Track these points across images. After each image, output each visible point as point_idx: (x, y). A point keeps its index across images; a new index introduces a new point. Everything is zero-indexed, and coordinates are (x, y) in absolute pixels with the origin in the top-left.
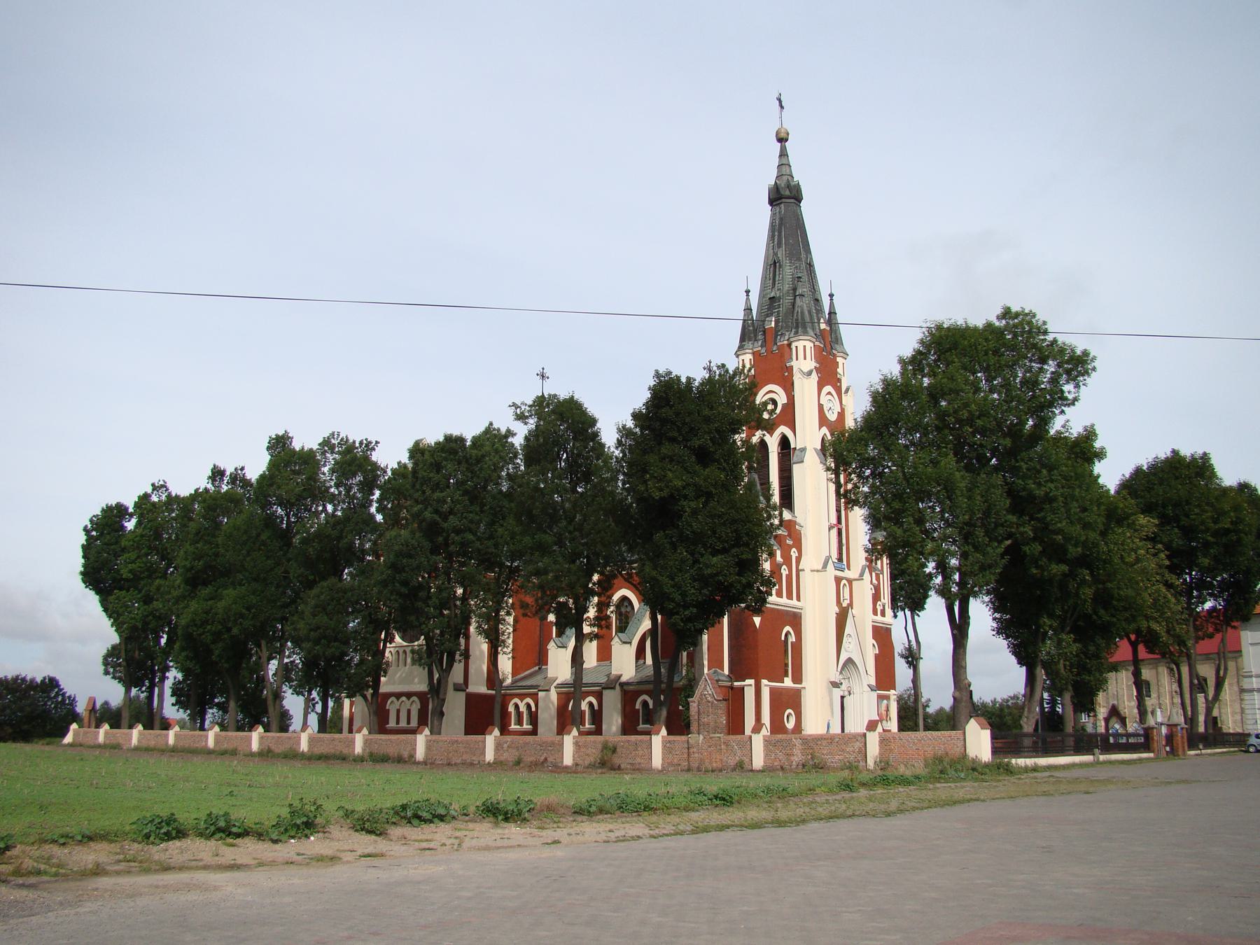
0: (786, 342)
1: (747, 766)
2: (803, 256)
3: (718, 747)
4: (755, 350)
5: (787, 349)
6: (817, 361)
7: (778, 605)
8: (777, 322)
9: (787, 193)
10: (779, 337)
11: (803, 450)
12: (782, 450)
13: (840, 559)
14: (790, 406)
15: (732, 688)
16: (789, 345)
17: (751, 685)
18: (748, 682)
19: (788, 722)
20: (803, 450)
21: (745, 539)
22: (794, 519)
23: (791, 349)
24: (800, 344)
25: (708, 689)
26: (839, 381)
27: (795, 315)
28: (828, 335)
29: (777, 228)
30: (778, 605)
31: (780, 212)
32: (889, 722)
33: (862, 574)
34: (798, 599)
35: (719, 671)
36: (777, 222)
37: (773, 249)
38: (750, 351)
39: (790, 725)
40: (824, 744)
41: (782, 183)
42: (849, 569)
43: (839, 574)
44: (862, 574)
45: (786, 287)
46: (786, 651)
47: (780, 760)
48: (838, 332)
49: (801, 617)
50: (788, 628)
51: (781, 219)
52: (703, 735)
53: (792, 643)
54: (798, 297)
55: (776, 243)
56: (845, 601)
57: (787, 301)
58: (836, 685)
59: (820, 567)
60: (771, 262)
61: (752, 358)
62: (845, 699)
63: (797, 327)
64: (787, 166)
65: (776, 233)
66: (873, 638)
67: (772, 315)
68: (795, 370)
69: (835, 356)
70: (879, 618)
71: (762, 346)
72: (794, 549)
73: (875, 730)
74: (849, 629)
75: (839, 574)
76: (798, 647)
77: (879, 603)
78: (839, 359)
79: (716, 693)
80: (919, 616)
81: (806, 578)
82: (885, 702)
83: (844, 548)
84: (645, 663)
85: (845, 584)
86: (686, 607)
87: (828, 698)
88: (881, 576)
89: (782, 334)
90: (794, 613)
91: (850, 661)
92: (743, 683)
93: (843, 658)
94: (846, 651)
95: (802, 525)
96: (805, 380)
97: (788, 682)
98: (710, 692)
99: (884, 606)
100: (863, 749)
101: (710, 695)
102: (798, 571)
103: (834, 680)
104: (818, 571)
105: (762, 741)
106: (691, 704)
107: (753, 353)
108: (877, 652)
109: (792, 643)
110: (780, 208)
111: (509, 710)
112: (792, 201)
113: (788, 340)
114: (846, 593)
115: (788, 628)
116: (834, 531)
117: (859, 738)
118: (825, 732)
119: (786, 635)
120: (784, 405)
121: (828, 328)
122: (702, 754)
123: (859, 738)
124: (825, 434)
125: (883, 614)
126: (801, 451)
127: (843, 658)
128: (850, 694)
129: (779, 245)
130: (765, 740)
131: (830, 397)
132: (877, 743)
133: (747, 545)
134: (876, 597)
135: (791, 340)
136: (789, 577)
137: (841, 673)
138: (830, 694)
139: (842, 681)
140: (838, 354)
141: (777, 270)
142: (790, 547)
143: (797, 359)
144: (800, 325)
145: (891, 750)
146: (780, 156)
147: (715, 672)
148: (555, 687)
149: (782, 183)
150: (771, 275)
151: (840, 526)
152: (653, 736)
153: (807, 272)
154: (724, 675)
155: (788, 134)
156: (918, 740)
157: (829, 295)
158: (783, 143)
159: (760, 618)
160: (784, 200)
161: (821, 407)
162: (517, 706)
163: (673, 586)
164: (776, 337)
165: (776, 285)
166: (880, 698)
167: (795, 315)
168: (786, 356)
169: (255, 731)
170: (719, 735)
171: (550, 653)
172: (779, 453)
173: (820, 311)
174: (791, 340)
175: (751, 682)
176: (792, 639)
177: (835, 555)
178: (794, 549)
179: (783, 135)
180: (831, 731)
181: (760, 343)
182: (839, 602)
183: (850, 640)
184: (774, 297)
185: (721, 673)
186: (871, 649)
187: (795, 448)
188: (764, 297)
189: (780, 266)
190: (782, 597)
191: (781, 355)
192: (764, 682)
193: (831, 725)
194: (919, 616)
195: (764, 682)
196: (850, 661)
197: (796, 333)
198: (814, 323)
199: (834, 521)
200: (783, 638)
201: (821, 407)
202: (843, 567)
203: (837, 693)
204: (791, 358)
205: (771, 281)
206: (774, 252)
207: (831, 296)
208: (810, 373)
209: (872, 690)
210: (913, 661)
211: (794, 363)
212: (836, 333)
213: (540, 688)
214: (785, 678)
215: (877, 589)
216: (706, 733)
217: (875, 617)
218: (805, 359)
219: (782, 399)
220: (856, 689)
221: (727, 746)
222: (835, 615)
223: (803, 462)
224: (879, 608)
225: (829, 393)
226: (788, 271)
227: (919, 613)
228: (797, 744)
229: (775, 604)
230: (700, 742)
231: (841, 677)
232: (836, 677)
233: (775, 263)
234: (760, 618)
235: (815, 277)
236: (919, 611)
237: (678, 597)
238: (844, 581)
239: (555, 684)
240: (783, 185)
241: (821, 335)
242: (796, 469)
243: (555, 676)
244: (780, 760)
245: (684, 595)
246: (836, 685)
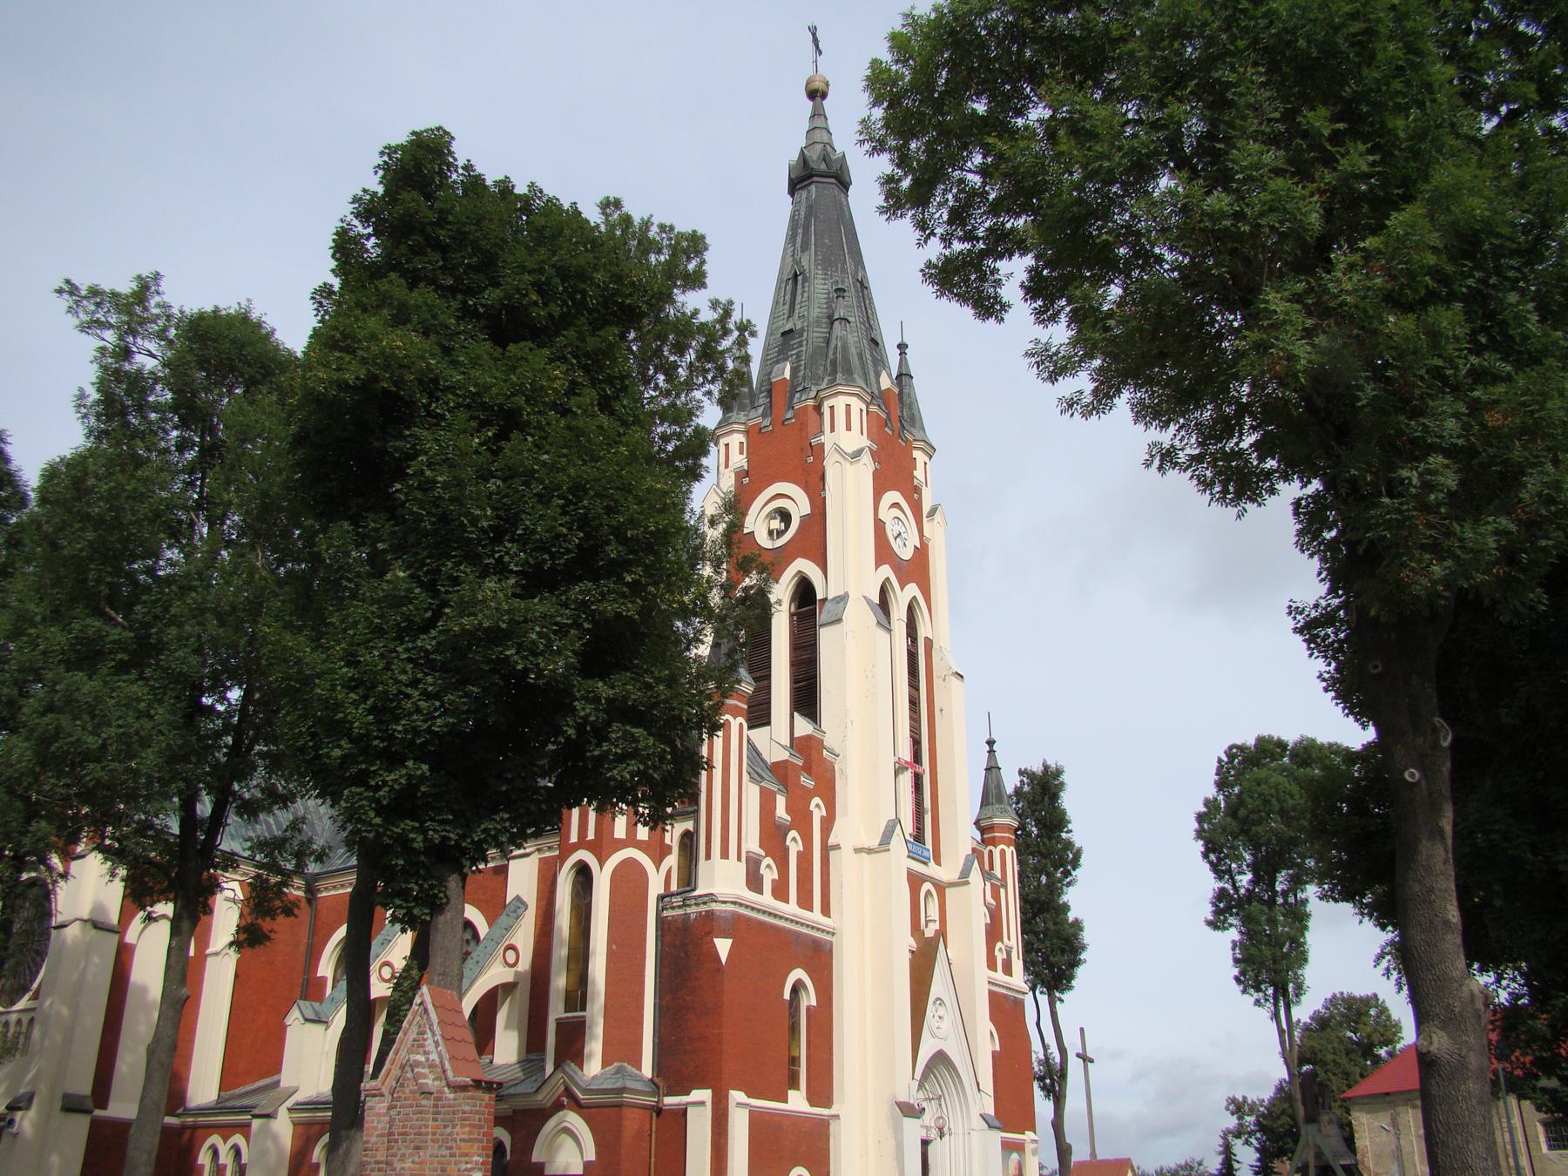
0: (811, 403)
4: (751, 423)
5: (812, 414)
6: (870, 437)
7: (776, 916)
8: (794, 371)
9: (823, 167)
11: (843, 599)
12: (799, 607)
15: (659, 1111)
16: (818, 409)
17: (702, 1103)
20: (843, 599)
22: (818, 735)
23: (821, 414)
24: (840, 403)
26: (917, 490)
29: (802, 222)
30: (776, 916)
33: (965, 873)
34: (826, 911)
35: (629, 1067)
36: (803, 213)
38: (742, 428)
41: (814, 155)
42: (938, 862)
43: (917, 867)
44: (965, 873)
45: (816, 312)
46: (794, 1029)
48: (915, 407)
49: (831, 951)
50: (798, 974)
51: (810, 208)
53: (809, 1008)
54: (837, 323)
55: (798, 245)
56: (931, 925)
58: (911, 1110)
59: (874, 843)
60: (788, 275)
62: (930, 1148)
63: (834, 372)
64: (824, 132)
65: (800, 231)
66: (992, 1019)
67: (785, 359)
68: (827, 448)
70: (999, 976)
71: (764, 416)
72: (816, 800)
74: (939, 986)
75: (917, 867)
76: (823, 1020)
77: (999, 945)
78: (917, 454)
79: (453, 1058)
80: (1062, 1001)
81: (846, 866)
82: (1015, 1156)
84: (491, 1062)
85: (928, 893)
86: (393, 760)
87: (891, 1143)
88: (1002, 891)
89: (804, 389)
90: (815, 941)
93: (927, 1049)
94: (934, 1035)
95: (837, 752)
96: (846, 465)
97: (797, 1101)
98: (434, 1057)
99: (1009, 954)
101: (432, 1066)
102: (826, 849)
104: (870, 851)
106: (370, 1103)
107: (747, 433)
108: (998, 1048)
109: (809, 1008)
111: (200, 1161)
112: (833, 180)
115: (798, 974)
119: (795, 990)
124: (888, 579)
125: (1008, 970)
127: (927, 1049)
129: (805, 247)
131: (896, 512)
134: (994, 933)
135: (822, 395)
136: (805, 858)
137: (921, 1086)
138: (897, 1130)
139: (924, 1104)
141: (799, 287)
142: (810, 794)
143: (832, 430)
147: (619, 1071)
148: (289, 1109)
149: (814, 155)
150: (788, 297)
151: (919, 770)
153: (857, 292)
154: (641, 1079)
157: (899, 346)
159: (729, 941)
160: (815, 179)
161: (879, 526)
162: (215, 1152)
164: (792, 397)
165: (797, 311)
166: (1008, 1147)
167: (831, 352)
168: (812, 427)
171: (290, 1033)
172: (792, 615)
173: (880, 362)
174: (822, 395)
175: (704, 1095)
176: (809, 999)
178: (816, 800)
179: (818, 85)
181: (761, 410)
182: (916, 928)
183: (941, 1011)
184: (791, 331)
185: (636, 1076)
186: (986, 1041)
188: (772, 334)
191: (802, 427)
192: (736, 1096)
194: (1062, 1001)
195: (736, 1096)
197: (832, 383)
198: (869, 379)
199: (906, 754)
201: (879, 526)
202: (926, 853)
203: (913, 1130)
204: (822, 432)
205: (787, 307)
207: (902, 347)
208: (857, 454)
210: (1052, 1084)
211: (827, 439)
212: (910, 408)
213: (256, 1111)
217: (992, 974)
218: (849, 428)
219: (800, 506)
220: (955, 1123)
222: (908, 956)
223: (839, 620)
224: (1000, 957)
225: (896, 505)
226: (819, 287)
227: (1062, 997)
231: (921, 1095)
233: (796, 276)
234: (729, 941)
235: (871, 302)
236: (1062, 992)
237: (359, 716)
238: (927, 886)
239: (289, 1103)
240: (815, 158)
241: (878, 397)
242: (827, 638)
243: (294, 1084)
246: (911, 1110)
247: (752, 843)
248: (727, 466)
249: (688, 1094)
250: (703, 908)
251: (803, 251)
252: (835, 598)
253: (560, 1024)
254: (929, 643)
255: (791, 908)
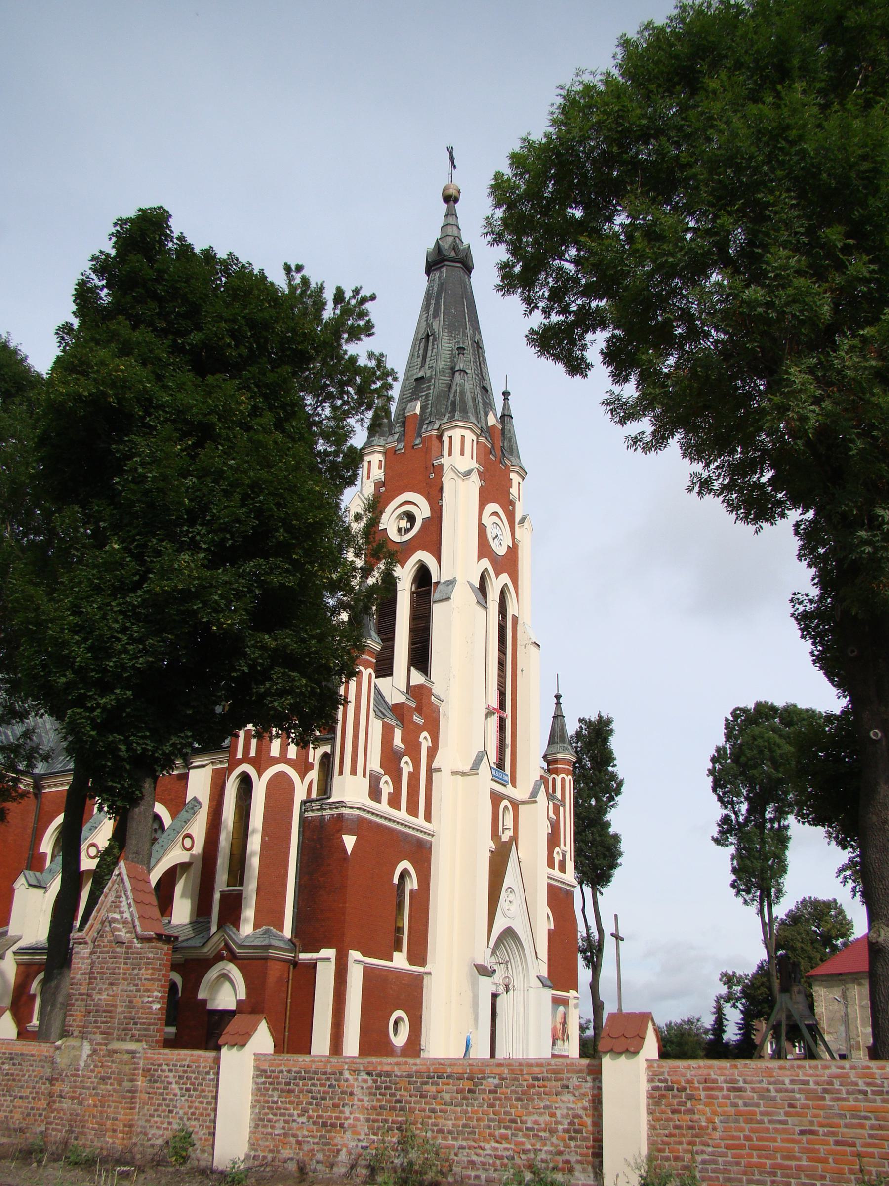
0: (435, 433)
1: (197, 1156)
2: (469, 331)
3: (127, 1085)
4: (388, 446)
5: (435, 442)
7: (390, 820)
8: (423, 408)
9: (453, 254)
10: (425, 427)
11: (451, 583)
12: (418, 587)
13: (500, 765)
14: (435, 523)
15: (295, 963)
16: (440, 437)
17: (328, 959)
18: (325, 953)
19: (395, 1034)
20: (451, 583)
21: (281, 534)
22: (428, 685)
24: (456, 434)
25: (124, 905)
26: (512, 503)
27: (452, 395)
28: (498, 435)
30: (390, 820)
31: (439, 277)
32: (566, 1043)
33: (534, 794)
34: (428, 818)
36: (435, 289)
37: (426, 321)
38: (381, 449)
39: (400, 1039)
40: (447, 1097)
41: (446, 244)
44: (534, 794)
45: (442, 364)
46: (400, 906)
47: (299, 1143)
49: (430, 848)
50: (405, 864)
51: (441, 285)
52: (91, 1042)
53: (412, 891)
54: (457, 373)
55: (431, 313)
56: (506, 832)
57: (441, 381)
58: (484, 971)
59: (467, 768)
61: (382, 458)
63: (453, 411)
65: (433, 302)
69: (508, 471)
70: (556, 873)
71: (398, 441)
72: (425, 734)
73: (636, 1053)
74: (510, 879)
76: (422, 899)
77: (557, 849)
79: (141, 917)
82: (561, 1009)
83: (508, 752)
84: (170, 922)
85: (506, 808)
88: (561, 809)
89: (430, 422)
91: (509, 933)
92: (314, 956)
94: (505, 915)
95: (442, 698)
97: (400, 961)
98: (127, 915)
99: (564, 856)
100: (589, 1121)
101: (125, 922)
102: (430, 771)
103: (482, 963)
104: (463, 774)
105: (251, 1072)
109: (412, 891)
110: (441, 272)
113: (438, 429)
114: (508, 820)
115: (405, 864)
116: (494, 721)
117: (575, 1081)
118: (359, 447)
120: (425, 520)
121: (500, 427)
122: (80, 1103)
123: (575, 1081)
124: (486, 569)
125: (562, 869)
126: (448, 585)
128: (507, 991)
129: (436, 315)
130: (260, 1072)
131: (495, 519)
132: (643, 1101)
133: (283, 550)
134: (553, 840)
136: (414, 778)
137: (493, 953)
138: (474, 986)
139: (495, 967)
140: (512, 468)
141: (430, 344)
142: (420, 729)
143: (450, 454)
144: (458, 408)
145: (697, 1132)
146: (446, 216)
147: (266, 932)
148: (15, 953)
149: (446, 244)
150: (421, 352)
152: (224, 1050)
154: (282, 939)
155: (459, 192)
156: (811, 1095)
157: (504, 394)
158: (452, 203)
160: (447, 263)
161: (482, 529)
163: (76, 629)
165: (427, 363)
166: (557, 1002)
167: (452, 395)
168: (434, 452)
169: (242, 1045)
170: (132, 1046)
171: (17, 894)
172: (412, 593)
173: (489, 405)
175: (330, 953)
176: (412, 884)
177: (493, 756)
179: (452, 191)
180: (473, 1054)
181: (396, 436)
182: (495, 835)
184: (422, 377)
186: (544, 921)
187: (438, 582)
189: (435, 339)
190: (399, 810)
191: (427, 450)
192: (354, 955)
193: (472, 1042)
194: (602, 894)
195: (354, 955)
196: (509, 933)
197: (452, 419)
199: (494, 703)
200: (396, 880)
201: (482, 529)
203: (487, 986)
205: (420, 359)
206: (427, 324)
207: (506, 394)
208: (468, 474)
209: (544, 986)
211: (446, 461)
212: (510, 441)
214: (395, 954)
215: (555, 827)
216: (99, 1038)
217: (550, 871)
218: (462, 453)
219: (422, 511)
220: (518, 982)
221: (153, 1081)
222: (489, 854)
223: (448, 599)
224: (557, 858)
225: (495, 514)
226: (445, 345)
227: (601, 889)
228: (356, 1090)
229: (386, 818)
230: (82, 1064)
231: (493, 960)
232: (484, 957)
233: (428, 336)
235: (484, 357)
237: (80, 654)
238: (505, 803)
239: (15, 948)
241: (486, 432)
242: (438, 611)
244: (299, 1143)
245: (101, 650)
246: (484, 971)
247: (375, 764)
248: (368, 478)
249: (318, 952)
250: (335, 812)
251: (434, 317)
252: (446, 582)
253: (224, 895)
254: (515, 619)
255: (402, 815)
